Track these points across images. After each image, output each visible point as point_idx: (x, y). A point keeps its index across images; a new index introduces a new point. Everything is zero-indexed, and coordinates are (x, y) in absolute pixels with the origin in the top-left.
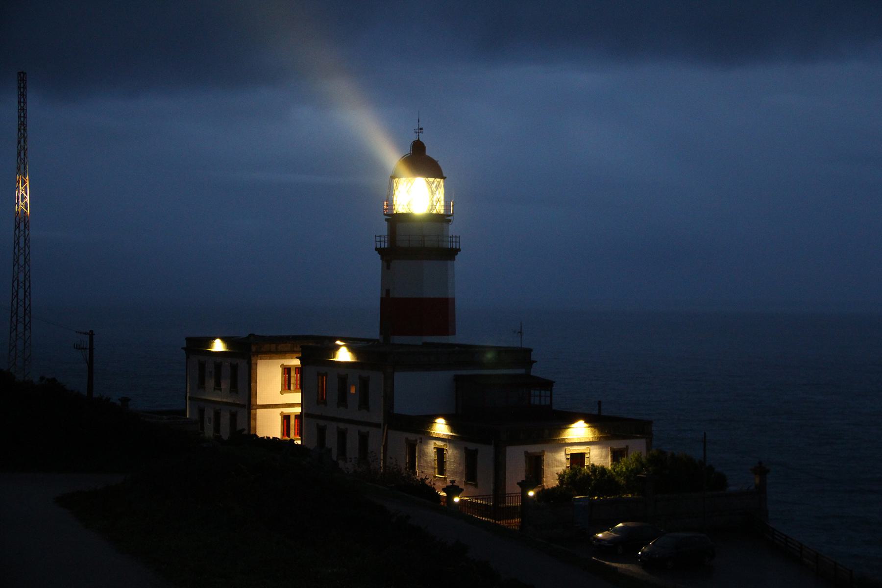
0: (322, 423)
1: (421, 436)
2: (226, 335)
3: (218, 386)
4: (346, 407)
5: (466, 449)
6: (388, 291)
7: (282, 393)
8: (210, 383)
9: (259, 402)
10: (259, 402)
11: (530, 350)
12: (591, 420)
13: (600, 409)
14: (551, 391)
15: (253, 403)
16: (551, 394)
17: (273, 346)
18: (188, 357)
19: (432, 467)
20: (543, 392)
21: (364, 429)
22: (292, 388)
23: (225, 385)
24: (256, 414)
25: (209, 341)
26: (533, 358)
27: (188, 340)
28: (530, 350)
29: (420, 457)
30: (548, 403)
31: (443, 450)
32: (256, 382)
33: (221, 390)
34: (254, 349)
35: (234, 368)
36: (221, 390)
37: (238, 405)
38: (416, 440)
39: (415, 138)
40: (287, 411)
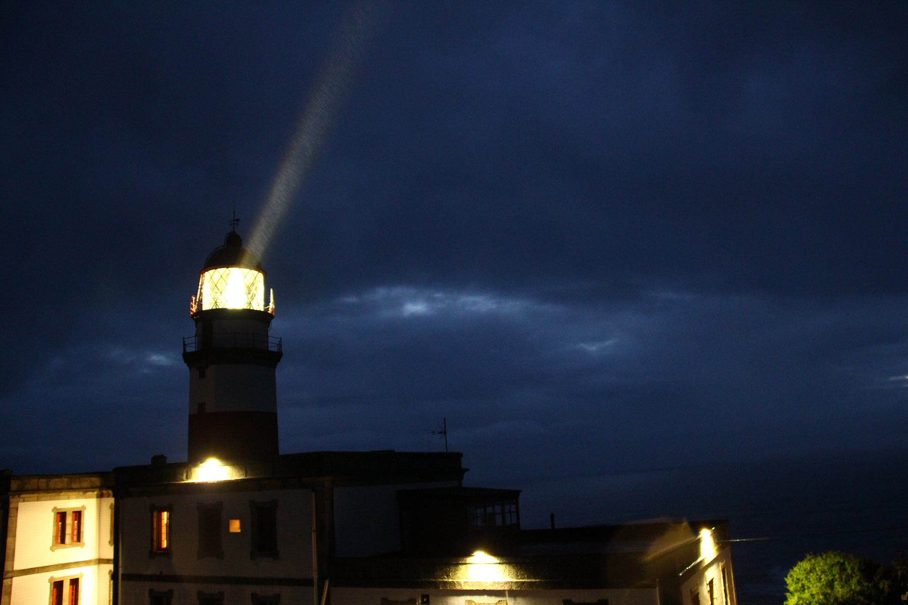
1: (421, 591)
6: (202, 406)
7: (52, 549)
9: (550, 527)
10: (550, 527)
12: (503, 550)
14: (517, 504)
16: (184, 349)
17: (43, 482)
20: (507, 508)
21: (163, 587)
22: (68, 539)
30: (514, 522)
32: (15, 536)
34: (14, 485)
37: (227, 580)
40: (58, 575)
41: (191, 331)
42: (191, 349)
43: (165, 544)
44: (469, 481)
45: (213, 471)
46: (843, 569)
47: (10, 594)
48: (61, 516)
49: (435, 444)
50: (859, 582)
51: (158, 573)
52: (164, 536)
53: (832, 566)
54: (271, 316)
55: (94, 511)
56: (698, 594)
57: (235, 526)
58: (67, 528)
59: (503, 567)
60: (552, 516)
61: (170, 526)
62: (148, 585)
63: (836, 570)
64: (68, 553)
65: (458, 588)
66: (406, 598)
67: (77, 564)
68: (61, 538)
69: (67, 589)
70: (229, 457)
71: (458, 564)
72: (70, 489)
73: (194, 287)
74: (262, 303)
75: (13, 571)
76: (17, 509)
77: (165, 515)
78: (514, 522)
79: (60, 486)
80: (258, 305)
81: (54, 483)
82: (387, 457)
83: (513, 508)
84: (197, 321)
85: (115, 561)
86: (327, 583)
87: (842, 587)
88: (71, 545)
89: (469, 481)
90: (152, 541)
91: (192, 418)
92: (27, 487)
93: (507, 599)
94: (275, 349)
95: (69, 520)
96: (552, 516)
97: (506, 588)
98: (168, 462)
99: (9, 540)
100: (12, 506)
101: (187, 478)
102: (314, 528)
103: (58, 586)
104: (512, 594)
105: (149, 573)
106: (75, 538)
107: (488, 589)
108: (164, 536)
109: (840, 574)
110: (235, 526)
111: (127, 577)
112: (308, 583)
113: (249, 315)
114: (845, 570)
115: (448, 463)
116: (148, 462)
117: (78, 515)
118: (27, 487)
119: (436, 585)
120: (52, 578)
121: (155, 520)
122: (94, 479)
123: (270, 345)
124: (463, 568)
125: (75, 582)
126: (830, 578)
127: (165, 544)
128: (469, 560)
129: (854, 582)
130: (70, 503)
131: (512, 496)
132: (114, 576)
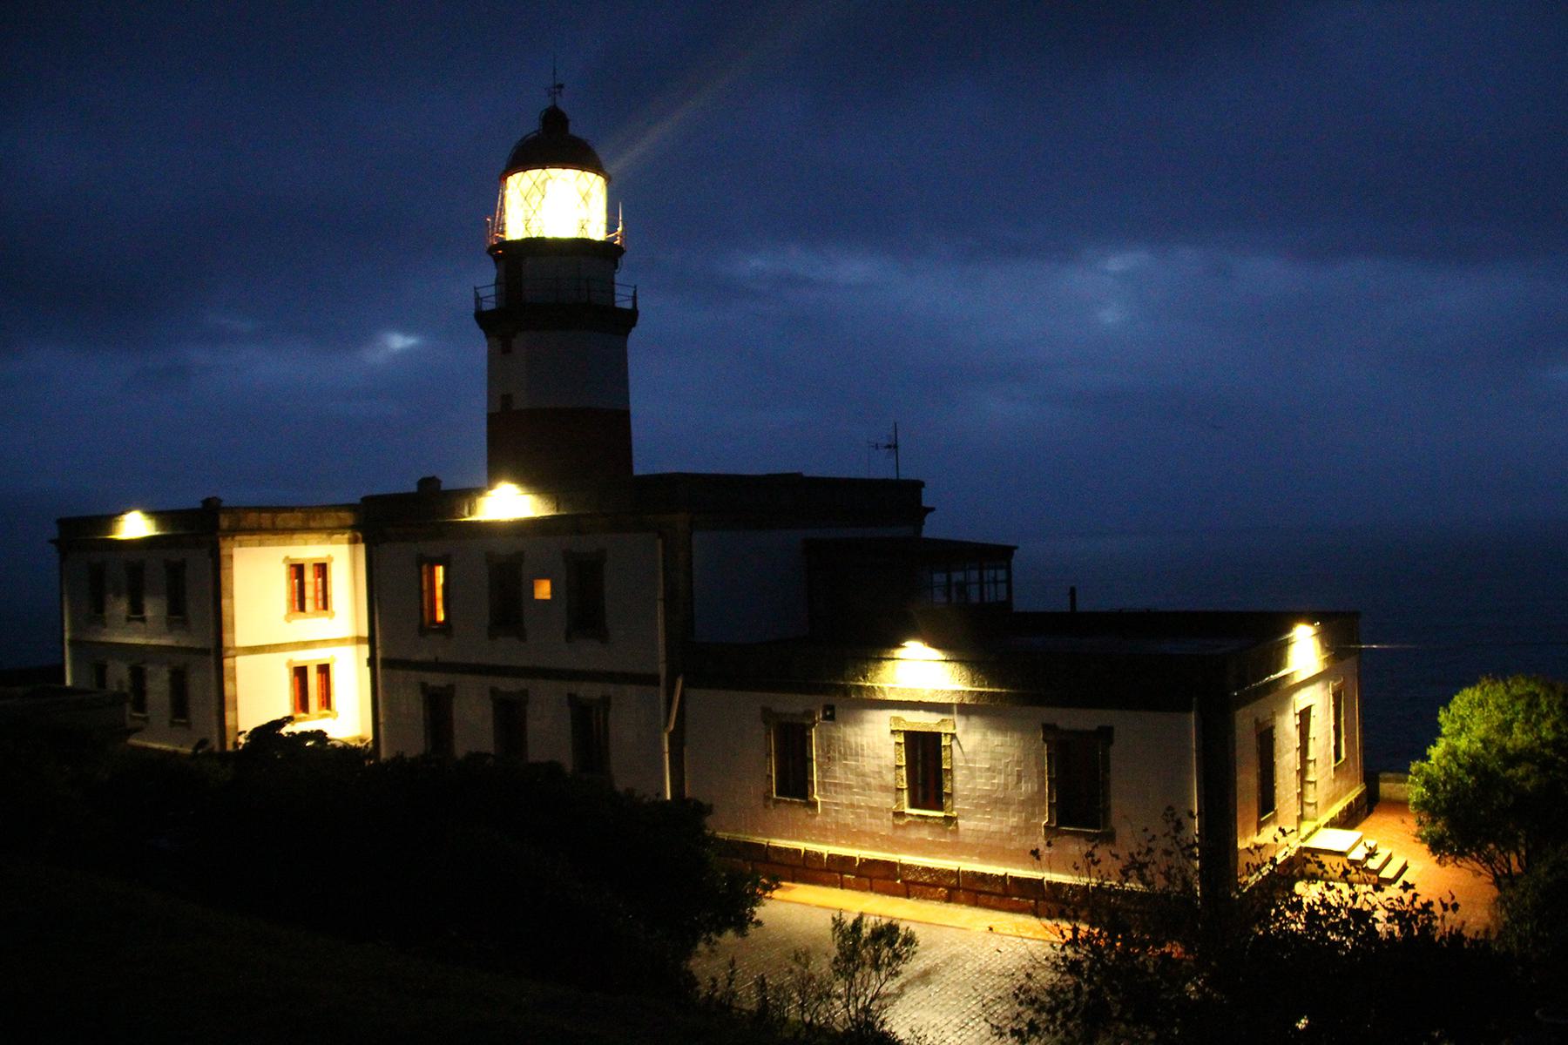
0: (436, 680)
1: (824, 699)
2: (163, 508)
3: (137, 610)
4: (521, 635)
5: (1049, 729)
6: (507, 399)
8: (121, 607)
11: (918, 485)
13: (1073, 600)
15: (227, 642)
16: (1009, 574)
17: (266, 518)
18: (63, 559)
19: (884, 788)
22: (309, 604)
23: (154, 608)
24: (234, 669)
25: (109, 519)
26: (926, 503)
27: (63, 523)
28: (918, 485)
29: (828, 758)
30: (1003, 596)
31: (936, 737)
33: (143, 620)
34: (224, 522)
35: (176, 573)
36: (143, 620)
38: (810, 714)
39: (548, 103)
41: (485, 280)
42: (489, 305)
43: (441, 617)
44: (933, 528)
45: (507, 503)
46: (1533, 703)
47: (234, 679)
48: (298, 570)
49: (881, 469)
50: (1555, 727)
51: (431, 658)
52: (440, 605)
53: (1518, 698)
54: (619, 251)
55: (343, 560)
56: (1272, 728)
57: (543, 590)
58: (307, 588)
59: (951, 667)
60: (1073, 592)
61: (446, 587)
62: (415, 676)
63: (1520, 705)
64: (311, 626)
65: (880, 696)
66: (801, 709)
67: (325, 642)
68: (300, 603)
69: (313, 679)
70: (533, 480)
71: (880, 660)
72: (307, 529)
73: (492, 202)
74: (603, 228)
75: (234, 648)
76: (231, 557)
77: (440, 571)
78: (1003, 596)
79: (292, 524)
80: (598, 233)
81: (282, 519)
82: (793, 482)
83: (1002, 575)
84: (497, 259)
85: (371, 640)
86: (680, 682)
87: (1524, 732)
88: (314, 614)
89: (933, 528)
90: (422, 609)
91: (492, 419)
92: (244, 524)
93: (956, 717)
94: (628, 305)
95: (309, 576)
96: (1073, 592)
97: (954, 701)
98: (444, 487)
99: (225, 602)
100: (224, 552)
101: (470, 513)
102: (660, 595)
103: (301, 673)
104: (964, 710)
105: (417, 657)
106: (320, 604)
107: (925, 700)
108: (440, 605)
109: (1526, 712)
110: (543, 590)
111: (389, 664)
112: (653, 680)
113: (581, 248)
114: (1538, 705)
115: (904, 498)
116: (414, 489)
117: (322, 569)
118: (244, 524)
119: (845, 691)
120: (290, 662)
121: (425, 578)
122: (342, 514)
123: (617, 298)
124: (888, 666)
125: (324, 670)
126: (1508, 717)
127: (441, 617)
128: (898, 653)
129: (1547, 724)
130: (310, 550)
131: (1002, 555)
132: (372, 662)
